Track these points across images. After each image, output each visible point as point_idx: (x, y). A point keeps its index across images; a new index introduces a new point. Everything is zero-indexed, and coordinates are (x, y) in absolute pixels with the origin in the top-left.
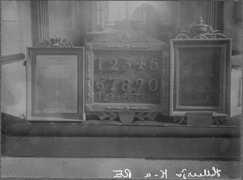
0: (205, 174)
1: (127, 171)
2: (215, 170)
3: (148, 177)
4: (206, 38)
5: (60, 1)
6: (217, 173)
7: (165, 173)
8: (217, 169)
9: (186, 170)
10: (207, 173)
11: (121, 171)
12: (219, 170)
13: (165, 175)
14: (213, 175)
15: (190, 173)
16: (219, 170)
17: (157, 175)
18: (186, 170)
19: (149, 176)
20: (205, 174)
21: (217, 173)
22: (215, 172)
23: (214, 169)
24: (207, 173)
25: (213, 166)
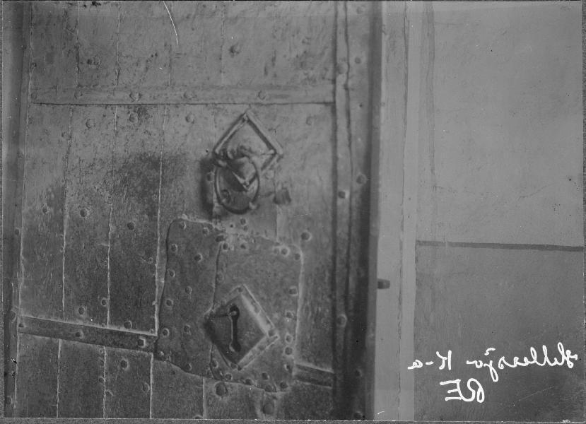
0: (546, 359)
1: (473, 385)
2: (562, 352)
3: (557, 365)
4: (481, 393)
5: (584, 395)
6: (567, 359)
7: (446, 358)
8: (569, 352)
9: (438, 353)
10: (541, 359)
11: (458, 382)
12: (572, 354)
13: (446, 361)
14: (556, 362)
15: (503, 357)
16: (572, 354)
17: (431, 363)
18: (438, 353)
19: (418, 367)
20: (535, 361)
21: (567, 359)
22: (564, 358)
23: (562, 347)
24: (541, 359)
25: (531, 346)
